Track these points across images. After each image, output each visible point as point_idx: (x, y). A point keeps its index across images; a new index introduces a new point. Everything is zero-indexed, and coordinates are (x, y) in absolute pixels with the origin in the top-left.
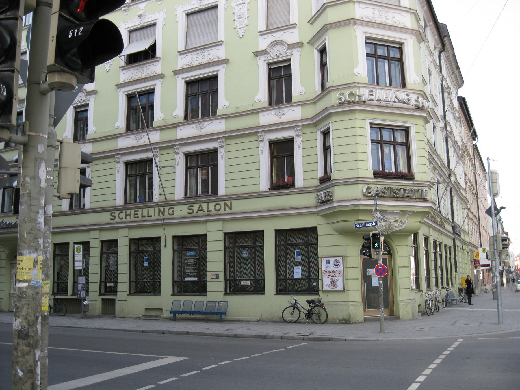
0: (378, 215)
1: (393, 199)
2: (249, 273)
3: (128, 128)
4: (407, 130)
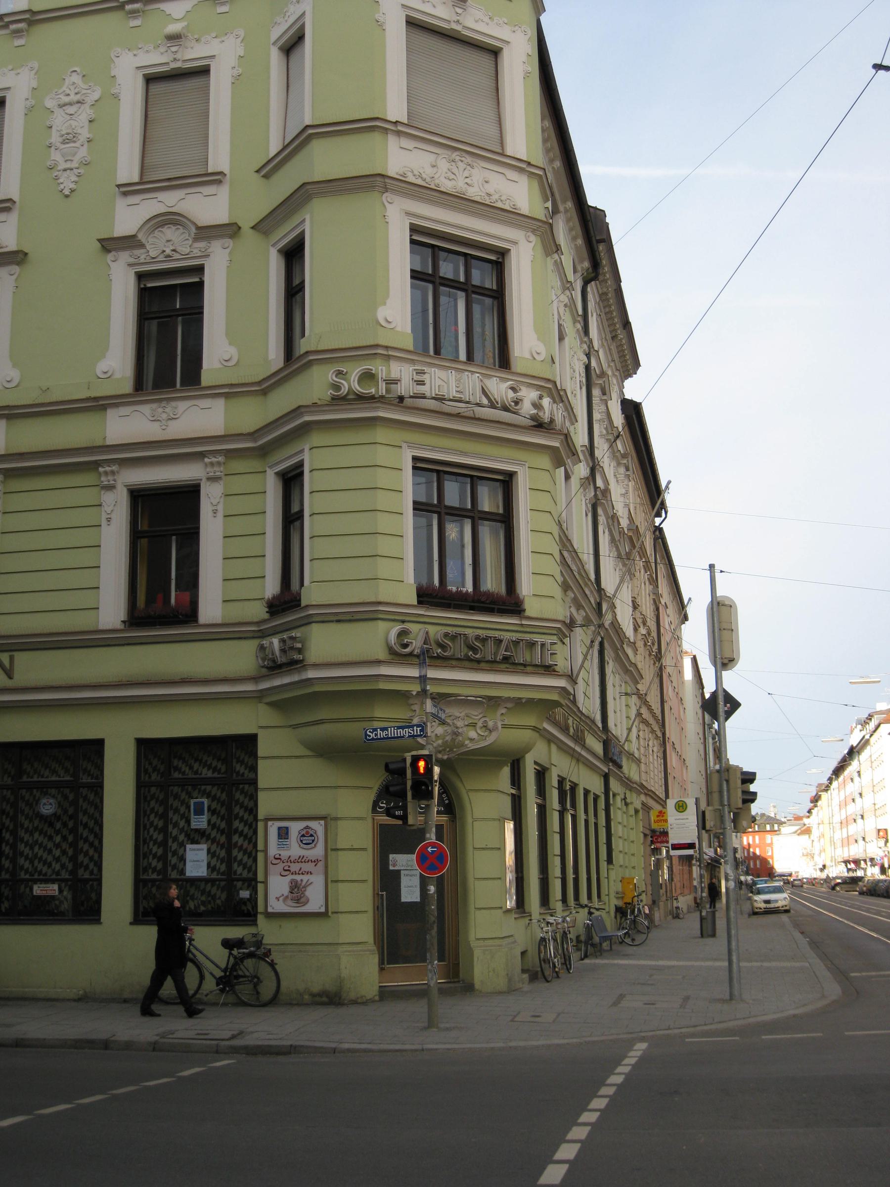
0: (429, 706)
1: (467, 664)
2: (58, 860)
4: (506, 483)
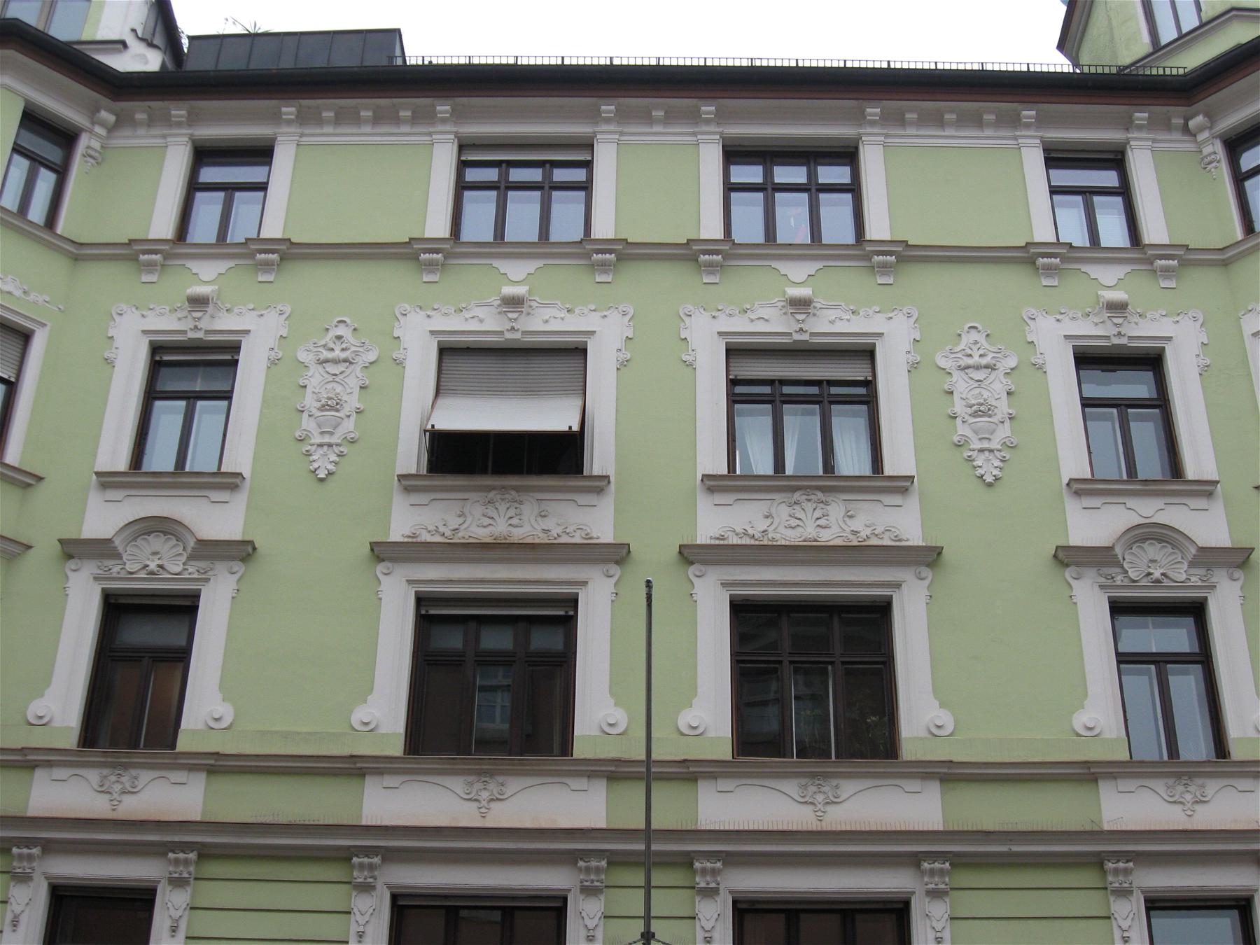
3: (91, 734)
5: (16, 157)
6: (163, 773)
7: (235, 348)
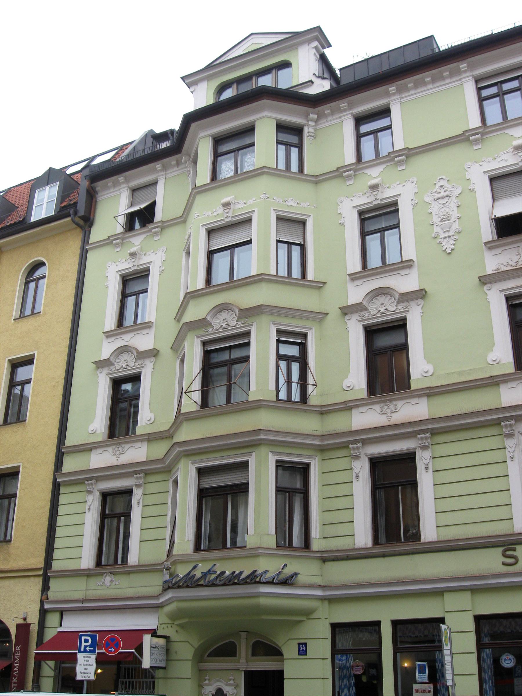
3: (372, 390)
5: (279, 146)
6: (408, 401)
7: (396, 203)
